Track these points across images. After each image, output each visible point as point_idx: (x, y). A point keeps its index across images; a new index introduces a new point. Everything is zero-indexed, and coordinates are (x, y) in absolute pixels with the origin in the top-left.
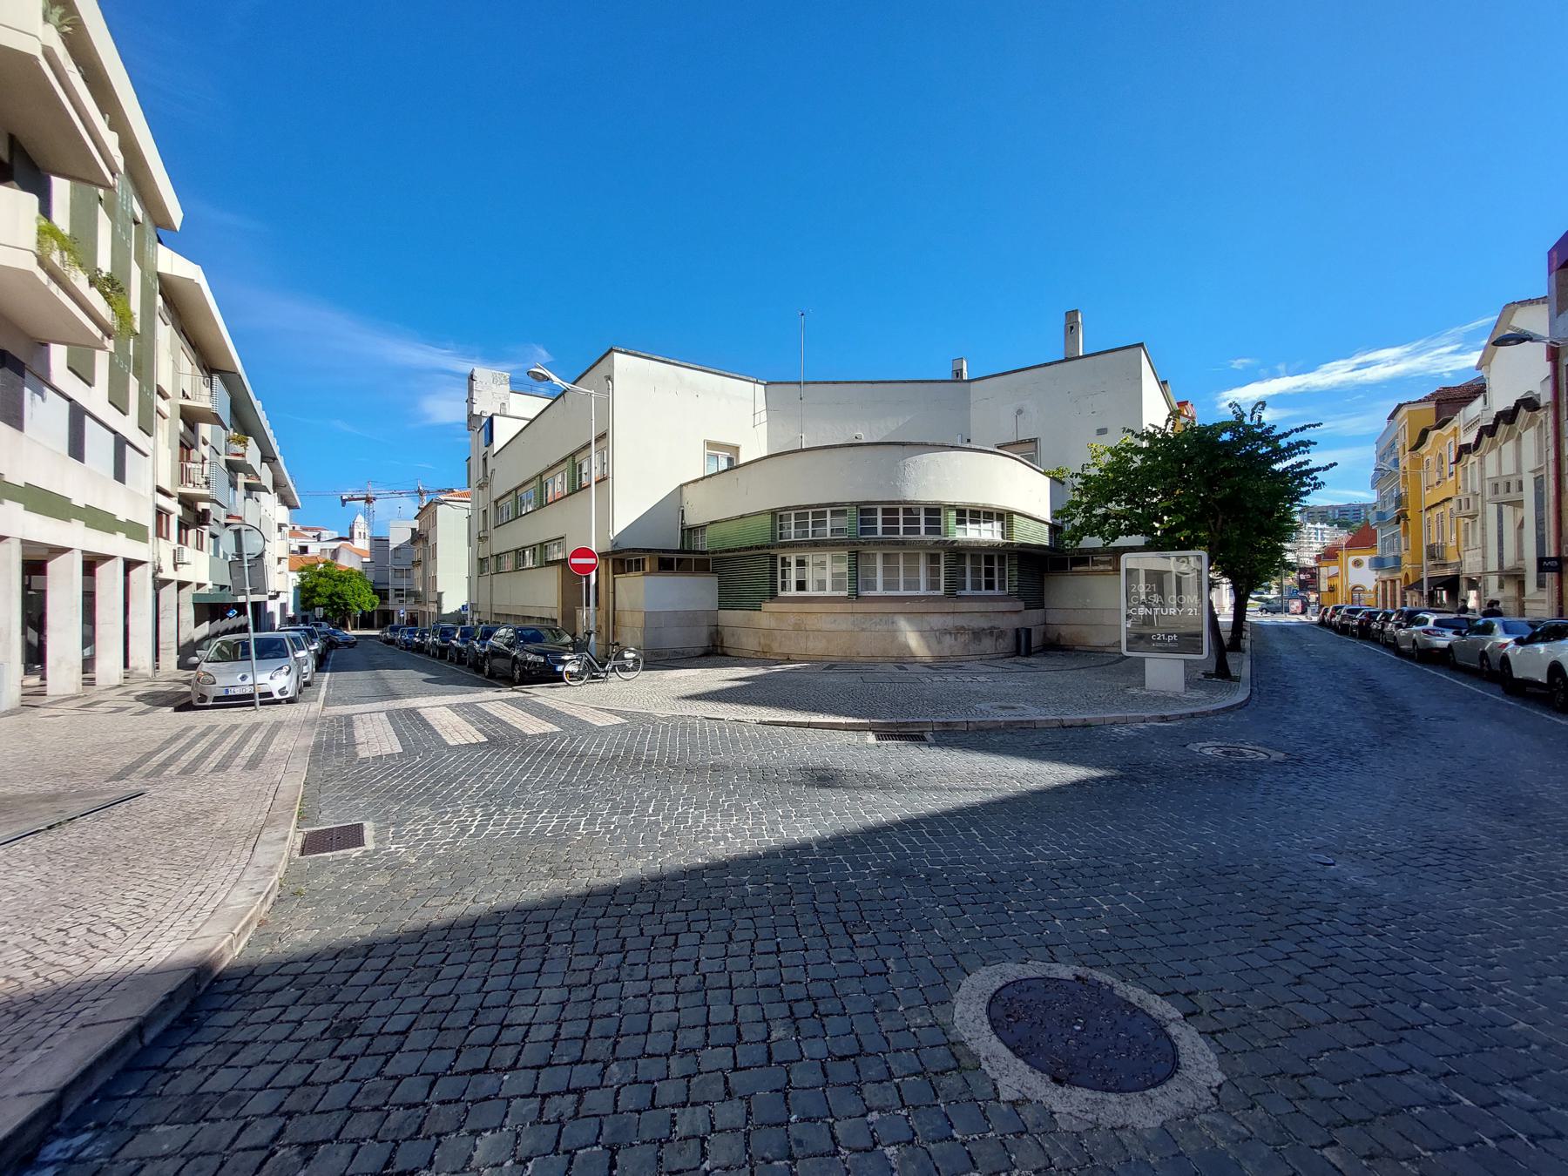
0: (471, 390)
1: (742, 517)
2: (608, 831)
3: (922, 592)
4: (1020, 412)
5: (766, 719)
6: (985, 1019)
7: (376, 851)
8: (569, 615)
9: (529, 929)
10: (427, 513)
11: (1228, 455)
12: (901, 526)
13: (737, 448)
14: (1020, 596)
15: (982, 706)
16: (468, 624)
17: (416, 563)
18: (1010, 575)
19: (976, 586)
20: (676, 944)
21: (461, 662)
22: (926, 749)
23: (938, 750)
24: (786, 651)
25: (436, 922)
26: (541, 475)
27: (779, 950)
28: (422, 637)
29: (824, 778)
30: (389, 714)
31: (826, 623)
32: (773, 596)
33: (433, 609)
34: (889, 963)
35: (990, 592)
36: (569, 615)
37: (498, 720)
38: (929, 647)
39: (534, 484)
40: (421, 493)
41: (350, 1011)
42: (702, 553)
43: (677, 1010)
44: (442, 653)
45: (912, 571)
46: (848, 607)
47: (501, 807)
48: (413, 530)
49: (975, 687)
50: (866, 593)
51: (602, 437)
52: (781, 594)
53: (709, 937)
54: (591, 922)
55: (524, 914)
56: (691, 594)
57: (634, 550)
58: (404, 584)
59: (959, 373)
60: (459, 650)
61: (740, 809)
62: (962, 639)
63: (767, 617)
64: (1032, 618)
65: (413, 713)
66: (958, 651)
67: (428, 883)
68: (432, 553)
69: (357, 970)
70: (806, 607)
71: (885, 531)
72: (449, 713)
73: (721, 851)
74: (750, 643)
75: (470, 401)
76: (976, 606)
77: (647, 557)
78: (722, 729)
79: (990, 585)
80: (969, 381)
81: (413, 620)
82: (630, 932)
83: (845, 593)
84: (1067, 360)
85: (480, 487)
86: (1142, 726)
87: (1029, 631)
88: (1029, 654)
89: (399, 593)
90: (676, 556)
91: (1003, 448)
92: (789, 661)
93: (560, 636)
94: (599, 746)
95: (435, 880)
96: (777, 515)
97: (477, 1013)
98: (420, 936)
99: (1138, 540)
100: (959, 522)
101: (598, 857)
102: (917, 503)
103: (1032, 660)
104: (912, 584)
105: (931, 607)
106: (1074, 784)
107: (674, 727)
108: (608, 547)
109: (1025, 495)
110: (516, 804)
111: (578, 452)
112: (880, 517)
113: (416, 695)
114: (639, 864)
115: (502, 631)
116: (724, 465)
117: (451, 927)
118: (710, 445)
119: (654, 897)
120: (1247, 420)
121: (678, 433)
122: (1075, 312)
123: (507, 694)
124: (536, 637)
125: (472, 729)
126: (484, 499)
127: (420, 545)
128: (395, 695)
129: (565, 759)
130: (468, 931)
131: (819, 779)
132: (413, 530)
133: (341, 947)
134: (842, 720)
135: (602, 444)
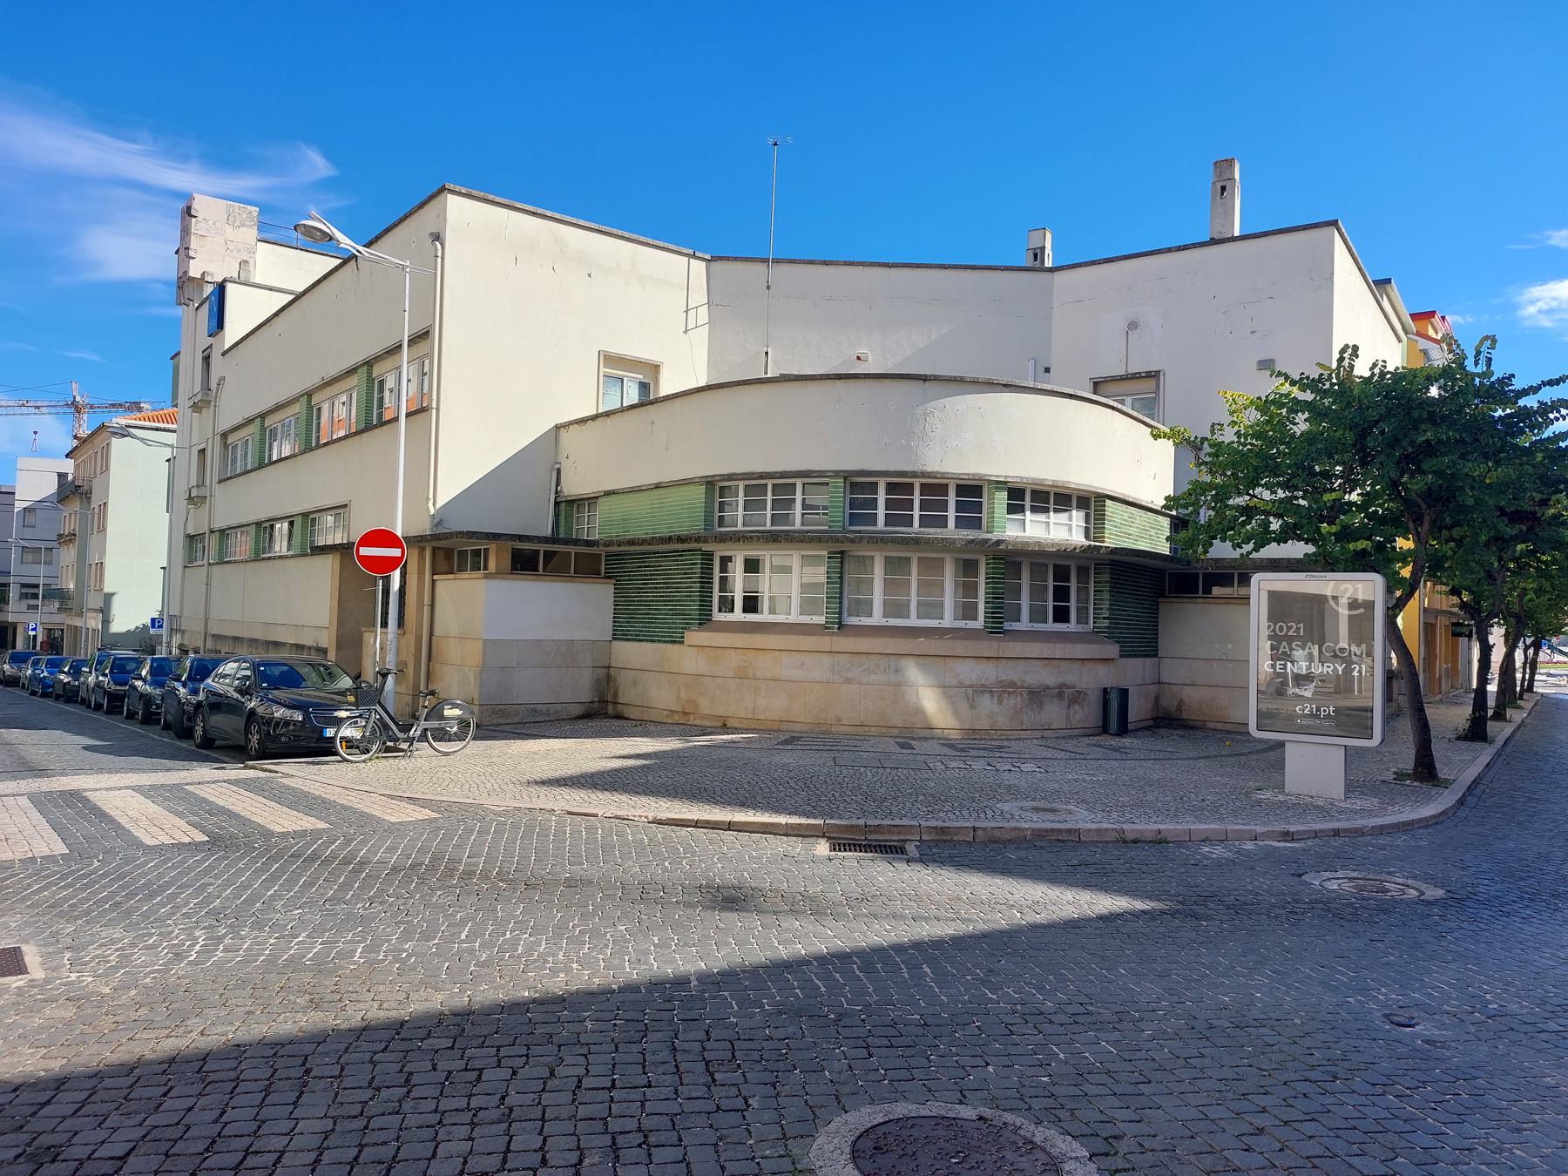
0: (185, 232)
1: (658, 486)
2: (397, 959)
3: (948, 621)
4: (1133, 325)
5: (663, 816)
6: (848, 1150)
7: (47, 981)
8: (351, 643)
9: (280, 1063)
10: (90, 447)
11: (1433, 419)
12: (916, 513)
13: (655, 368)
14: (1112, 634)
15: (1006, 807)
16: (162, 653)
17: (66, 539)
18: (1092, 603)
19: (1037, 615)
20: (479, 1079)
21: (150, 718)
22: (902, 866)
23: (919, 867)
24: (721, 711)
25: (150, 1056)
26: (309, 394)
27: (613, 1086)
28: (76, 671)
29: (731, 899)
30: (35, 799)
31: (787, 668)
32: (704, 620)
33: (94, 622)
34: (750, 1101)
35: (1061, 627)
36: (351, 643)
37: (223, 811)
38: (956, 713)
39: (296, 408)
40: (77, 408)
41: (45, 1140)
42: (589, 543)
43: (471, 1139)
44: (114, 703)
45: (931, 587)
46: (824, 642)
47: (234, 930)
48: (62, 476)
49: (1012, 779)
50: (854, 621)
51: (420, 337)
52: (719, 616)
53: (524, 1073)
54: (367, 1057)
55: (275, 1049)
56: (568, 611)
57: (471, 535)
58: (39, 574)
59: (1038, 254)
60: (146, 699)
61: (596, 934)
62: (1013, 702)
63: (692, 655)
64: (1132, 673)
65: (75, 798)
66: (1003, 721)
67: (134, 1016)
68: (97, 521)
69: (48, 1103)
70: (758, 640)
71: (889, 520)
72: (138, 797)
73: (558, 984)
74: (662, 697)
75: (184, 252)
76: (1035, 649)
77: (493, 547)
78: (591, 830)
79: (1061, 615)
80: (1051, 270)
81: (53, 643)
82: (418, 1065)
83: (821, 620)
84: (1214, 242)
85: (196, 407)
86: (1249, 846)
87: (1124, 693)
88: (1123, 730)
89: (29, 591)
90: (542, 548)
91: (1103, 388)
92: (725, 728)
93: (332, 676)
94: (392, 849)
95: (143, 1011)
96: (718, 487)
97: (214, 1142)
98: (132, 1071)
99: (1297, 549)
100: (1012, 509)
101: (381, 988)
102: (943, 476)
103: (1126, 741)
104: (931, 608)
105: (960, 647)
106: (1101, 918)
107: (515, 826)
108: (425, 528)
109: (1131, 470)
110: (258, 926)
111: (378, 358)
112: (882, 497)
113: (78, 771)
114: (440, 997)
115: (230, 667)
116: (632, 396)
117: (172, 1061)
118: (609, 359)
119: (455, 1031)
120: (1470, 365)
121: (550, 335)
122: (1230, 162)
123: (235, 772)
124: (291, 678)
125: (182, 823)
126: (202, 430)
127: (75, 505)
128: (39, 772)
129: (334, 864)
130: (198, 1065)
131: (725, 900)
132: (62, 476)
133: (20, 1081)
134: (782, 819)
135: (422, 348)
